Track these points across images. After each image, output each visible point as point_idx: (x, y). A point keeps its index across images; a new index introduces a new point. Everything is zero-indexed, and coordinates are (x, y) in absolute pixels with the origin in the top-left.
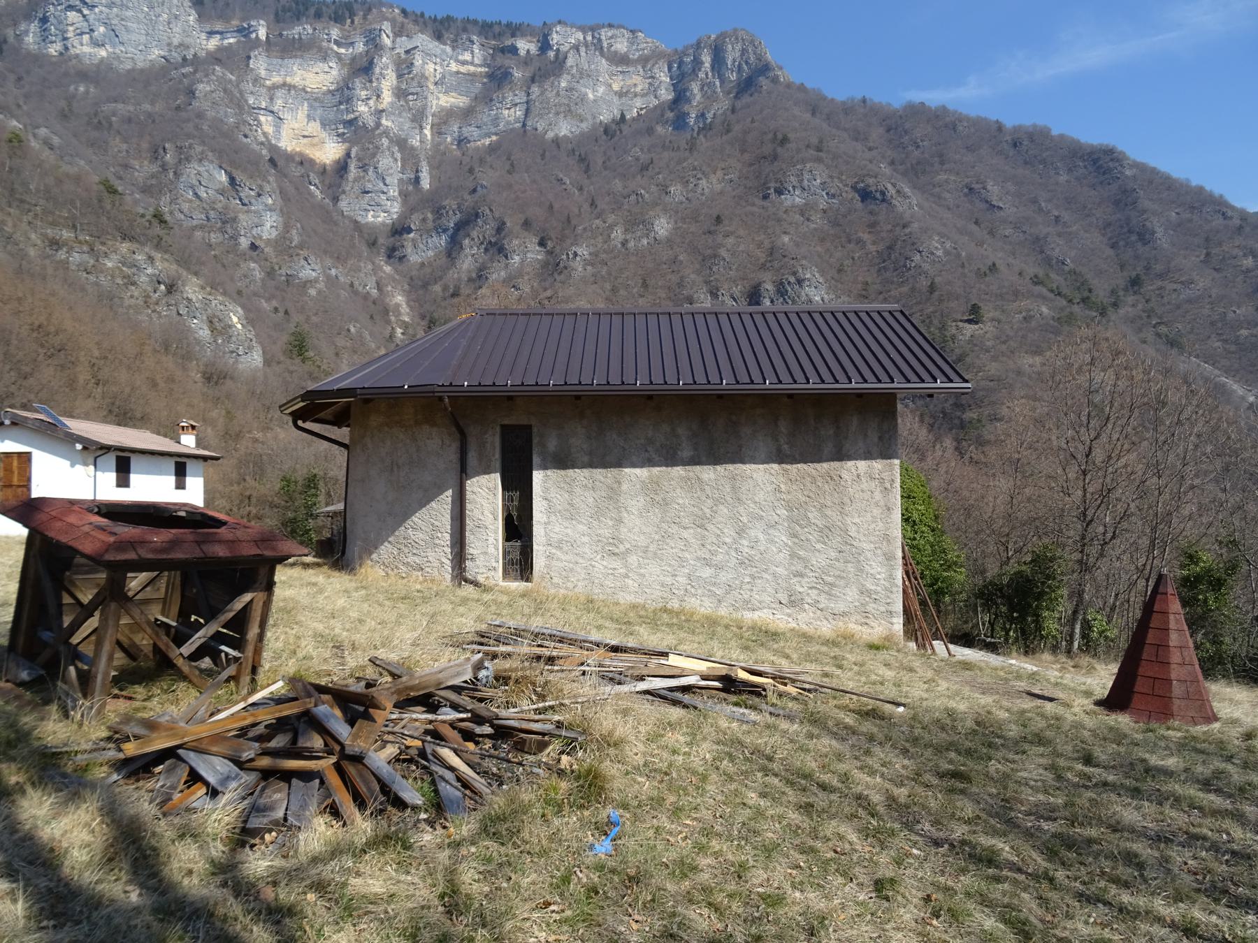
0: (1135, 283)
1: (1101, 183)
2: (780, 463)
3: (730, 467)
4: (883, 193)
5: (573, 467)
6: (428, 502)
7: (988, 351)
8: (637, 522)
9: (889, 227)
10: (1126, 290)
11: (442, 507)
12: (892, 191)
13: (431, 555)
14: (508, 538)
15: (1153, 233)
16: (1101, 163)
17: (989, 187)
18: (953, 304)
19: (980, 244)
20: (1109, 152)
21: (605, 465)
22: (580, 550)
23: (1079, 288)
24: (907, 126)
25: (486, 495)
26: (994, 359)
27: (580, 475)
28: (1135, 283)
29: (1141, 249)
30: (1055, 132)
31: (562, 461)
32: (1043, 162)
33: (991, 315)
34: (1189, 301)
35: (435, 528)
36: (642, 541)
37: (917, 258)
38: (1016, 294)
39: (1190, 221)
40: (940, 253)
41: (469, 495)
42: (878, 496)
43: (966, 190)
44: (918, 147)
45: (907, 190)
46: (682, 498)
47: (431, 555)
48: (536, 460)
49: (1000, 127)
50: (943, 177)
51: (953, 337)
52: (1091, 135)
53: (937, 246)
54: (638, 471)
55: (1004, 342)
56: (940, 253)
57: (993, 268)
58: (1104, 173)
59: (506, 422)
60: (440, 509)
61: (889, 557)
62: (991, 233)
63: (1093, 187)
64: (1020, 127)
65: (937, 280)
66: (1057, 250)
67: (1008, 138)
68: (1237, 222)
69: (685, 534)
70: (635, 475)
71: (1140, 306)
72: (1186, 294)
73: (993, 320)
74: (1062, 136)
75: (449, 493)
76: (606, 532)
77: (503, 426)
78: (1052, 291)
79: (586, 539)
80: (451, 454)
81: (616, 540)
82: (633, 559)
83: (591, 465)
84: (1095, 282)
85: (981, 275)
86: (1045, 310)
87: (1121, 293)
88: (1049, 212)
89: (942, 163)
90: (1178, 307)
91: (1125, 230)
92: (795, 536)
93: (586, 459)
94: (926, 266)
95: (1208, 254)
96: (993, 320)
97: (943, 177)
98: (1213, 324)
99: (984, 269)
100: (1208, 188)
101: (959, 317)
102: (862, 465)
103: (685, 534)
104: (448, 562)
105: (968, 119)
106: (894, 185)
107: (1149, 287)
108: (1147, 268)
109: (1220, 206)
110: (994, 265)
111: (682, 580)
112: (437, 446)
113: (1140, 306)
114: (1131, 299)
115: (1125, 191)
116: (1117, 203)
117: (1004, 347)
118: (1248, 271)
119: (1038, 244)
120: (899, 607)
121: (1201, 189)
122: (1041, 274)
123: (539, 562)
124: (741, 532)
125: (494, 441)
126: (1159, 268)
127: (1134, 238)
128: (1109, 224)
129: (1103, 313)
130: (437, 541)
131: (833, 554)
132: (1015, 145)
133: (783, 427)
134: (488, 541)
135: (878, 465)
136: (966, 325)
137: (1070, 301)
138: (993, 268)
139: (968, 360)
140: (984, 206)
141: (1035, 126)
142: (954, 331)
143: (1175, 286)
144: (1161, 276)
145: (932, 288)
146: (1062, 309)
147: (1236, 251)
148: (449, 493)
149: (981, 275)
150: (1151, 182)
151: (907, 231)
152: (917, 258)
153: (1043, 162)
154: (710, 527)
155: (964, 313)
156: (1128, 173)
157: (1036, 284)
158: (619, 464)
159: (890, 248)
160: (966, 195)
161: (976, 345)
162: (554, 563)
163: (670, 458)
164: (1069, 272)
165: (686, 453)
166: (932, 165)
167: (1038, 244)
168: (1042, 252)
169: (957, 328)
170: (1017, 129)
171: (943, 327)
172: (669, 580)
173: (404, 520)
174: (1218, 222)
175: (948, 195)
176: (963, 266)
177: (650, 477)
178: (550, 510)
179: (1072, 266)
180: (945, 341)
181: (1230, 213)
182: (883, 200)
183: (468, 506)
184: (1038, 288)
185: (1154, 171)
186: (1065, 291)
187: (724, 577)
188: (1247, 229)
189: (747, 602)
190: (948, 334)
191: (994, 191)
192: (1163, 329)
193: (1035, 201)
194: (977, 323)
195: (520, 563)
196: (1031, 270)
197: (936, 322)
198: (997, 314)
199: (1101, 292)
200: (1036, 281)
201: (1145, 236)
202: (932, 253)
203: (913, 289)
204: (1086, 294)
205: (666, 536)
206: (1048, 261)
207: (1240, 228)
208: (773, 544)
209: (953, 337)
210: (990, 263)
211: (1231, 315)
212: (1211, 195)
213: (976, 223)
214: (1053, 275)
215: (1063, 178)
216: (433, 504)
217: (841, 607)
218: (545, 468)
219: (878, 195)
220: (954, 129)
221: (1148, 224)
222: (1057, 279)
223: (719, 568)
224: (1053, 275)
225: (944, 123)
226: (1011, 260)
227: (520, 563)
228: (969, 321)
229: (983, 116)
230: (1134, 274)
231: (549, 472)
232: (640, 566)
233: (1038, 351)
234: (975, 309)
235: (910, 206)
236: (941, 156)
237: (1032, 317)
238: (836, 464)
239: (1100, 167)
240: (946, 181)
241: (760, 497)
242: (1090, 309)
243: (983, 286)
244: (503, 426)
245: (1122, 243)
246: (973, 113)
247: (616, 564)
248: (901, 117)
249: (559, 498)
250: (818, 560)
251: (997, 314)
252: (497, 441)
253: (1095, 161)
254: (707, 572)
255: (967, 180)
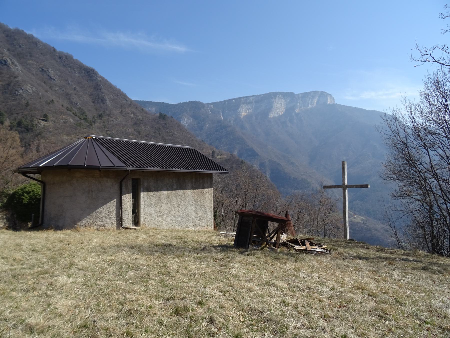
0: (100, 116)
1: (90, 80)
2: (193, 189)
3: (184, 191)
4: (5, 62)
5: (150, 191)
6: (106, 203)
7: (50, 132)
8: (165, 207)
9: (8, 76)
10: (97, 117)
11: (112, 205)
12: (9, 62)
13: (108, 221)
14: (133, 214)
15: (106, 101)
16: (90, 73)
17: (50, 71)
18: (36, 112)
19: (47, 91)
20: (93, 70)
21: (158, 191)
22: (152, 216)
23: (82, 114)
24: (16, 37)
25: (127, 200)
26: (53, 135)
27: (152, 193)
28: (100, 116)
29: (102, 105)
30: (75, 58)
31: (148, 190)
32: (70, 67)
33: (51, 119)
34: (116, 125)
35: (109, 212)
36: (166, 212)
37: (21, 91)
38: (61, 113)
39: (117, 99)
40: (31, 91)
41: (123, 201)
42: (210, 197)
43: (40, 69)
44: (20, 47)
45: (16, 63)
46: (174, 199)
47: (108, 221)
48: (142, 189)
49: (55, 50)
50: (31, 62)
51: (36, 125)
52: (88, 63)
53: (30, 89)
54: (165, 192)
55: (57, 130)
56: (31, 91)
57: (52, 101)
58: (91, 77)
59: (134, 178)
60: (112, 205)
61: (211, 212)
62: (50, 88)
63: (87, 80)
64: (62, 52)
65: (30, 102)
66: (75, 100)
67: (58, 55)
68: (129, 102)
69: (175, 209)
70: (165, 193)
71: (102, 124)
72: (116, 122)
73: (52, 121)
74: (77, 60)
75: (115, 200)
76: (158, 210)
77: (132, 179)
78: (74, 114)
79: (153, 212)
80: (116, 187)
81: (160, 212)
82: (164, 217)
83: (155, 191)
84: (87, 113)
85: (48, 103)
86: (71, 120)
87: (96, 118)
88: (72, 85)
89: (31, 56)
90: (113, 126)
91: (97, 98)
92: (196, 208)
93: (153, 189)
94: (24, 95)
95: (122, 111)
96: (52, 121)
97: (31, 62)
98: (123, 133)
99: (49, 101)
100: (122, 90)
101: (39, 118)
102: (207, 189)
103: (175, 209)
104: (115, 223)
105: (42, 43)
106: (11, 60)
107: (105, 118)
108: (104, 112)
109: (125, 97)
110: (53, 100)
111: (174, 221)
112: (110, 185)
113: (102, 124)
114: (99, 121)
115: (97, 85)
116: (95, 88)
117: (57, 132)
118: (132, 118)
119: (68, 96)
120: (213, 224)
121: (119, 90)
122: (69, 107)
123: (142, 220)
124: (186, 208)
125: (130, 183)
126: (108, 112)
127: (100, 101)
128: (92, 95)
129: (91, 125)
130: (110, 216)
131: (202, 212)
132: (60, 58)
133: (194, 180)
134: (128, 216)
135: (210, 189)
136: (42, 121)
137: (80, 119)
138: (52, 101)
139: (42, 134)
140: (48, 78)
141: (67, 53)
142: (37, 123)
143: (112, 119)
144: (108, 115)
145: (27, 105)
146: (77, 121)
147: (129, 112)
148: (115, 200)
149: (48, 103)
150: (105, 84)
151: (17, 79)
152: (21, 91)
153: (70, 67)
154: (180, 207)
155: (41, 117)
156: (98, 79)
157: (68, 110)
158: (161, 190)
159: (9, 85)
160: (40, 71)
161: (46, 129)
162: (146, 220)
163: (172, 188)
164: (79, 108)
165: (175, 187)
166: (27, 56)
167: (68, 96)
168: (69, 99)
169: (38, 122)
170: (60, 53)
171: (32, 121)
172: (171, 222)
173: (95, 210)
174: (124, 101)
175: (33, 70)
176: (40, 98)
177: (168, 194)
178: (145, 205)
179: (80, 106)
180: (33, 126)
181: (128, 100)
182: (5, 65)
183: (123, 204)
184: (69, 112)
185: (106, 80)
186: (78, 115)
187: (183, 220)
188: (132, 106)
189: (187, 226)
190: (34, 124)
191: (52, 73)
192: (109, 132)
193: (67, 80)
194: (46, 121)
195: (136, 222)
196: (66, 105)
197: (29, 118)
198: (54, 119)
199: (90, 118)
200: (68, 109)
201: (103, 101)
202: (27, 91)
203: (19, 103)
204: (85, 117)
205: (171, 210)
206: (71, 103)
207: (130, 104)
208: (191, 210)
209: (36, 125)
210: (51, 99)
211: (128, 131)
212: (123, 93)
213: (45, 83)
214: (74, 108)
215: (77, 75)
216: (108, 204)
217: (203, 225)
218: (144, 192)
219: (3, 62)
220: (36, 44)
221: (105, 98)
222: (75, 110)
223: (182, 217)
224: (74, 108)
225: (33, 42)
226: (58, 99)
227: (136, 222)
228: (43, 120)
229: (48, 43)
230: (100, 113)
231: (145, 193)
232: (166, 219)
233: (68, 135)
234: (45, 116)
235: (18, 70)
236: (30, 53)
237: (67, 122)
238: (203, 189)
239: (89, 75)
240: (33, 64)
241: (190, 198)
242: (87, 122)
243: (48, 108)
244: (132, 179)
245: (96, 102)
246: (44, 41)
247: (160, 218)
248: (13, 33)
249: (147, 200)
250: (200, 214)
251: (54, 119)
252: (131, 182)
253: (88, 72)
254: (179, 219)
255: (41, 66)
